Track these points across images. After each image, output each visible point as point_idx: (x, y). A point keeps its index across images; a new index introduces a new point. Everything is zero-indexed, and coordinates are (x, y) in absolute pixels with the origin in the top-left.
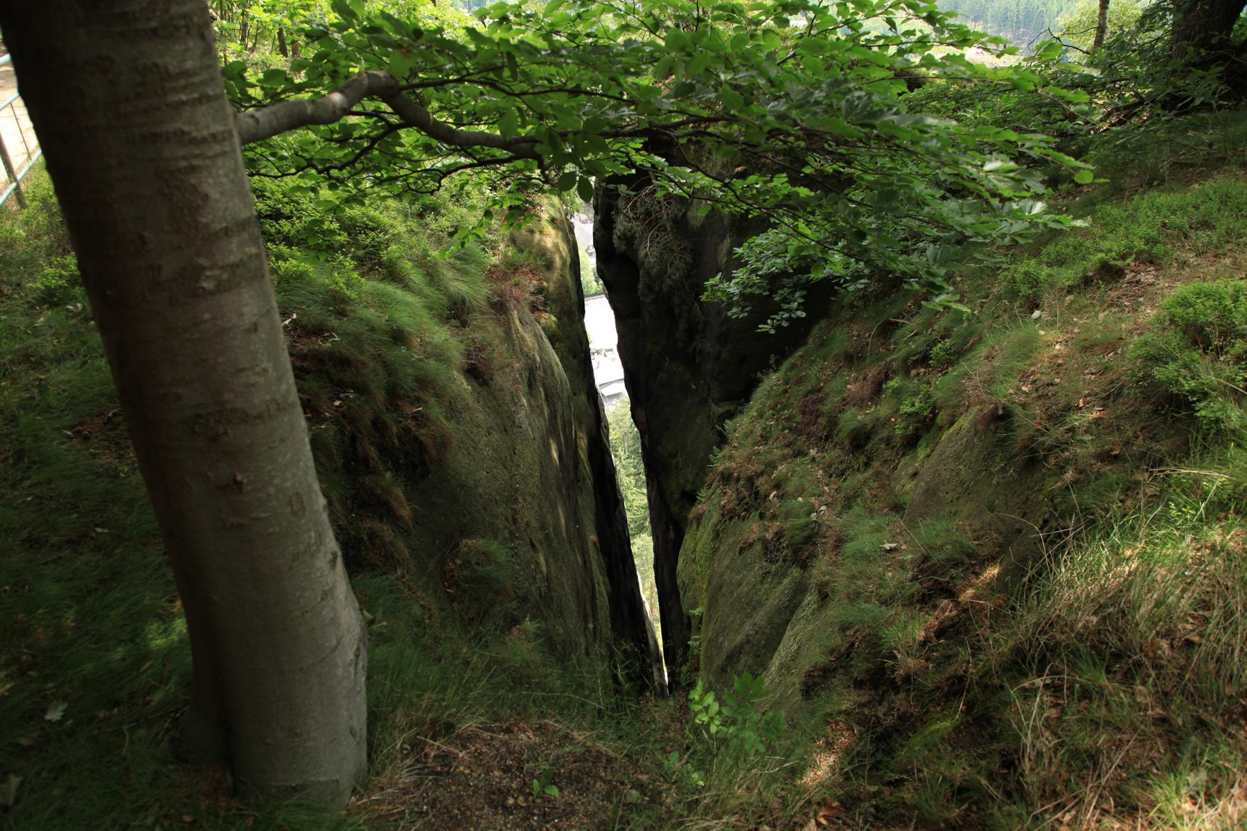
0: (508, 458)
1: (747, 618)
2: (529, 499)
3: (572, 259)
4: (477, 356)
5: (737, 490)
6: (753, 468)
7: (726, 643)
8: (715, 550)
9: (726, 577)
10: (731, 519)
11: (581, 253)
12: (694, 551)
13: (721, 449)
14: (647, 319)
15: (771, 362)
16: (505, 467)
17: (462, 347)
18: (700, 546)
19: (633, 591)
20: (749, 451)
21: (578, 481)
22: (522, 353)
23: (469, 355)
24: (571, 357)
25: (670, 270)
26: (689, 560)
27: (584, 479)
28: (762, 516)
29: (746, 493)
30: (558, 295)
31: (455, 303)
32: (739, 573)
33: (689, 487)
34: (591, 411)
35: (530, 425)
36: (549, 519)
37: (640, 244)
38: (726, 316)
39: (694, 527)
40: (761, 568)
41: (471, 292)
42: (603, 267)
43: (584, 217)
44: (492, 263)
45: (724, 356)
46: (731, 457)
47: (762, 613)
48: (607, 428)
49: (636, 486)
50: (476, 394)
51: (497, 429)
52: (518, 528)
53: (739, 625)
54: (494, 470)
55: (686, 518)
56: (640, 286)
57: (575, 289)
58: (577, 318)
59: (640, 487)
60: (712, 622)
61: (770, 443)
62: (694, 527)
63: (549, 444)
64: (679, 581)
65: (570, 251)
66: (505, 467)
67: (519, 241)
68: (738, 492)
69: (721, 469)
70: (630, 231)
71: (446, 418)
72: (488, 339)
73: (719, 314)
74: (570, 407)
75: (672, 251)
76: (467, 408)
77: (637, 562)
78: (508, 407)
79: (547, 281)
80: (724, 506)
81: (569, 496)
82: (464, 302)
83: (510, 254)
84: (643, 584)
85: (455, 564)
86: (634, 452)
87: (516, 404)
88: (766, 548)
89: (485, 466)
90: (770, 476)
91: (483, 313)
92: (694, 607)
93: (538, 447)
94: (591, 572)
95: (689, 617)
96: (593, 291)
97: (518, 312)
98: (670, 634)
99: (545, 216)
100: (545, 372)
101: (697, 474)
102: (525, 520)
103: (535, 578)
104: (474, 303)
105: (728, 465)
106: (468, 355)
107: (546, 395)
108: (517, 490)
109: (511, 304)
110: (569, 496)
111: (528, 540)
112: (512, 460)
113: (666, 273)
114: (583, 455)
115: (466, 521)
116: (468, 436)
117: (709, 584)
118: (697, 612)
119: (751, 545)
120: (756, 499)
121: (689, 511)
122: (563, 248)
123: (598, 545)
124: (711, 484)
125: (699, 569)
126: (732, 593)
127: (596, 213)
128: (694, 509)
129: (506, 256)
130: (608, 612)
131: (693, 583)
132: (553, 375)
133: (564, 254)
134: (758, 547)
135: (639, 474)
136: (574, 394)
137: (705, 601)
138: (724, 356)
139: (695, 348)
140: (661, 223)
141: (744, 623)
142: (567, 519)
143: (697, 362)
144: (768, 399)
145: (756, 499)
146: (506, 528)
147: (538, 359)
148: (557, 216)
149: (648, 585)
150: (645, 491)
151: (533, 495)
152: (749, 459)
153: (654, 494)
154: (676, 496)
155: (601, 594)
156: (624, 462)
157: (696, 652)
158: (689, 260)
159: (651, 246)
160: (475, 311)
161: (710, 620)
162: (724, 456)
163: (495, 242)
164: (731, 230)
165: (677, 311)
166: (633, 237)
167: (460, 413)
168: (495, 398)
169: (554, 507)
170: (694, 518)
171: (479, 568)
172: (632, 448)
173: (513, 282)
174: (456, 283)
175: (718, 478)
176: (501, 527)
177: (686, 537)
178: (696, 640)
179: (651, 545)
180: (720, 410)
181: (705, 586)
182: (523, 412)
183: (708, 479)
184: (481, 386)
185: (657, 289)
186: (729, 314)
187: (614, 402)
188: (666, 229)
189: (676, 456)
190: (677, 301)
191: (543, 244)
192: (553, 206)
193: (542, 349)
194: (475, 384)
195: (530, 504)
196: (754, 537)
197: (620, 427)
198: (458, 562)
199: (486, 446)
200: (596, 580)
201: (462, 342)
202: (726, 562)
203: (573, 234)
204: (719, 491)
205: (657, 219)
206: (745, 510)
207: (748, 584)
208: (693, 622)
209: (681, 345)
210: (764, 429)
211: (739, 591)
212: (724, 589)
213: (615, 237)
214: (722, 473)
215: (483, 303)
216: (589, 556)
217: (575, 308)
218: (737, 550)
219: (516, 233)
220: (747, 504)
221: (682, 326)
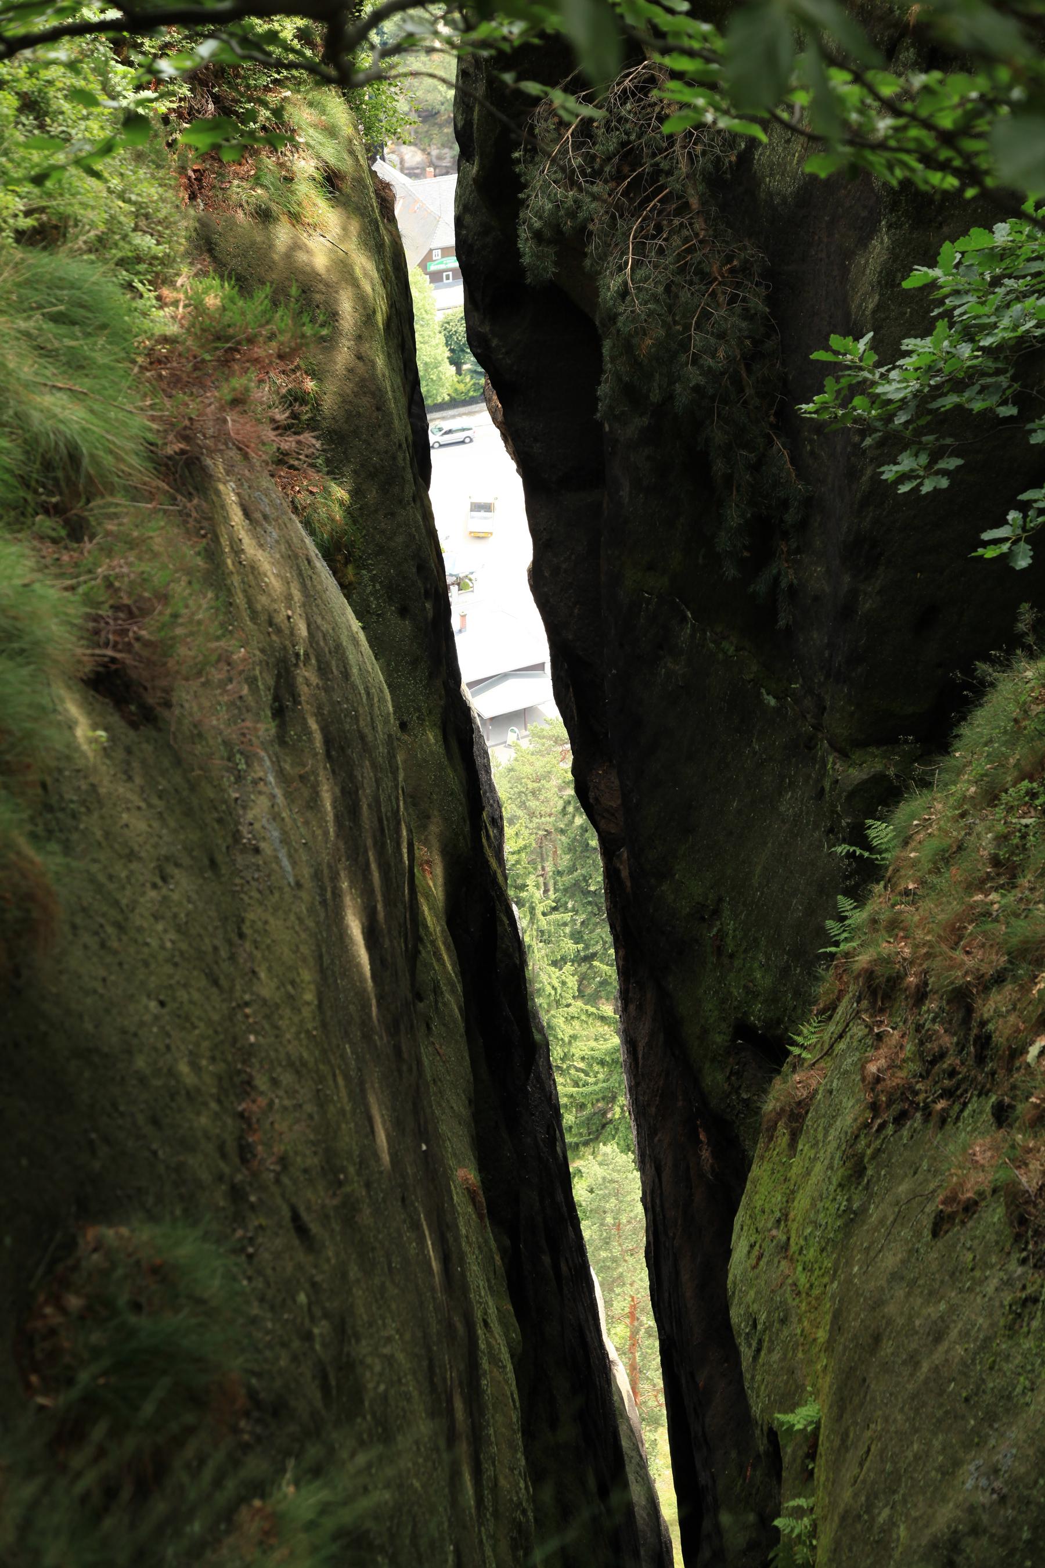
0: (224, 953)
1: (967, 1446)
2: (287, 1078)
3: (392, 305)
4: (124, 632)
5: (919, 1028)
6: (970, 962)
7: (902, 1531)
8: (852, 1219)
9: (890, 1309)
10: (900, 1119)
11: (416, 278)
12: (783, 1219)
13: (860, 898)
14: (625, 493)
15: (1021, 627)
16: (216, 983)
17: (76, 611)
18: (801, 1203)
19: (584, 1344)
20: (956, 906)
21: (419, 997)
22: (254, 615)
23: (97, 632)
24: (391, 613)
25: (697, 339)
26: (769, 1248)
27: (436, 990)
28: (1002, 1115)
29: (948, 1041)
30: (349, 416)
31: (48, 466)
32: (932, 1296)
33: (757, 1014)
34: (453, 779)
35: (285, 841)
36: (347, 1139)
37: (603, 257)
38: (876, 479)
39: (782, 1138)
40: (1008, 1283)
41: (97, 428)
42: (486, 329)
43: (413, 156)
44: (158, 330)
45: (867, 606)
46: (894, 925)
47: (1015, 1433)
48: (497, 822)
49: (581, 994)
50: (120, 754)
51: (186, 861)
52: (255, 1174)
53: (941, 1469)
54: (182, 995)
55: (752, 1109)
56: (604, 389)
57: (403, 401)
58: (409, 490)
59: (593, 999)
60: (853, 1457)
61: (1024, 881)
62: (782, 1138)
63: (337, 894)
64: (736, 1315)
65: (385, 280)
66: (216, 983)
67: (227, 245)
68: (923, 1037)
69: (863, 960)
70: (572, 214)
71: (33, 837)
72: (159, 578)
73: (852, 474)
74: (395, 772)
75: (705, 277)
76: (92, 798)
77: (588, 1231)
78: (220, 789)
79: (313, 374)
80: (878, 1080)
81: (398, 1050)
82: (74, 457)
83: (212, 301)
84: (608, 1304)
85: (63, 1310)
86: (577, 889)
87: (239, 778)
88: (1023, 1221)
89: (153, 982)
90: (1025, 989)
91: (135, 494)
92: (790, 1401)
93: (311, 910)
94: (465, 1288)
95: (772, 1435)
96: (443, 395)
97: (239, 482)
98: (703, 1478)
99: (305, 166)
100: (323, 670)
101: (785, 971)
102: (278, 1149)
103: (308, 1337)
104: (108, 461)
105: (885, 948)
106: (94, 636)
107: (328, 742)
108: (248, 1053)
109: (217, 466)
110: (398, 1050)
111: (286, 1213)
112: (232, 958)
113: (684, 346)
114: (432, 919)
115: (97, 1165)
116: (99, 888)
117: (837, 1325)
118: (800, 1418)
119: (970, 1208)
120: (981, 1060)
121: (763, 1088)
122: (364, 265)
123: (481, 1198)
124: (832, 1007)
125: (803, 1280)
126: (913, 1361)
127: (465, 155)
128: (777, 1084)
129: (197, 306)
130: (515, 1416)
131: (783, 1321)
132: (346, 675)
133: (368, 288)
134: (995, 1214)
135: (589, 958)
136: (403, 726)
137: (826, 1383)
138: (867, 606)
139: (776, 580)
140: (673, 184)
141: (957, 1463)
142: (397, 1125)
143: (782, 623)
144: (1011, 744)
145: (981, 1060)
146: (220, 1178)
147: (303, 630)
148: (346, 165)
149: (621, 1306)
150: (608, 1009)
151: (297, 1067)
152: (955, 934)
153: (644, 1029)
154: (719, 1039)
155: (494, 1360)
156: (543, 922)
157: (801, 1553)
158: (758, 304)
159: (637, 264)
160: (112, 490)
161: (844, 1445)
162: (874, 921)
163: (166, 261)
164: (894, 206)
165: (719, 466)
166: (582, 233)
167: (74, 816)
168: (178, 762)
169: (359, 1097)
170: (780, 1114)
171: (141, 1322)
172: (567, 879)
173: (225, 392)
174: (47, 400)
175: (853, 989)
176: (205, 1176)
177: (755, 1171)
178: (798, 1513)
179: (633, 1184)
180: (853, 774)
181: (822, 1335)
182: (263, 802)
183: (824, 989)
184: (134, 725)
185: (655, 397)
186: (889, 473)
187: (511, 737)
188: (686, 206)
189: (716, 913)
190: (718, 435)
191: (302, 257)
192: (331, 131)
193: (312, 597)
194: (115, 719)
195: (291, 1093)
196: (976, 1182)
197: (532, 815)
198: (74, 1302)
199: (156, 917)
200: (479, 1314)
201: (72, 588)
202: (890, 1260)
203: (392, 220)
204: (858, 1030)
205: (657, 172)
206: (948, 1094)
207: (965, 1335)
208: (788, 1451)
209: (731, 572)
210: (1002, 839)
211: (938, 1357)
212: (887, 1348)
213: (524, 233)
214: (869, 974)
215: (134, 461)
216: (457, 1239)
217: (404, 458)
218: (927, 1222)
219: (218, 221)
220: (952, 1073)
221: (734, 515)
